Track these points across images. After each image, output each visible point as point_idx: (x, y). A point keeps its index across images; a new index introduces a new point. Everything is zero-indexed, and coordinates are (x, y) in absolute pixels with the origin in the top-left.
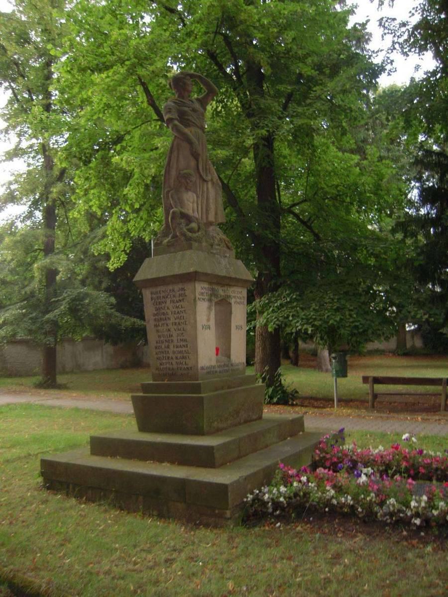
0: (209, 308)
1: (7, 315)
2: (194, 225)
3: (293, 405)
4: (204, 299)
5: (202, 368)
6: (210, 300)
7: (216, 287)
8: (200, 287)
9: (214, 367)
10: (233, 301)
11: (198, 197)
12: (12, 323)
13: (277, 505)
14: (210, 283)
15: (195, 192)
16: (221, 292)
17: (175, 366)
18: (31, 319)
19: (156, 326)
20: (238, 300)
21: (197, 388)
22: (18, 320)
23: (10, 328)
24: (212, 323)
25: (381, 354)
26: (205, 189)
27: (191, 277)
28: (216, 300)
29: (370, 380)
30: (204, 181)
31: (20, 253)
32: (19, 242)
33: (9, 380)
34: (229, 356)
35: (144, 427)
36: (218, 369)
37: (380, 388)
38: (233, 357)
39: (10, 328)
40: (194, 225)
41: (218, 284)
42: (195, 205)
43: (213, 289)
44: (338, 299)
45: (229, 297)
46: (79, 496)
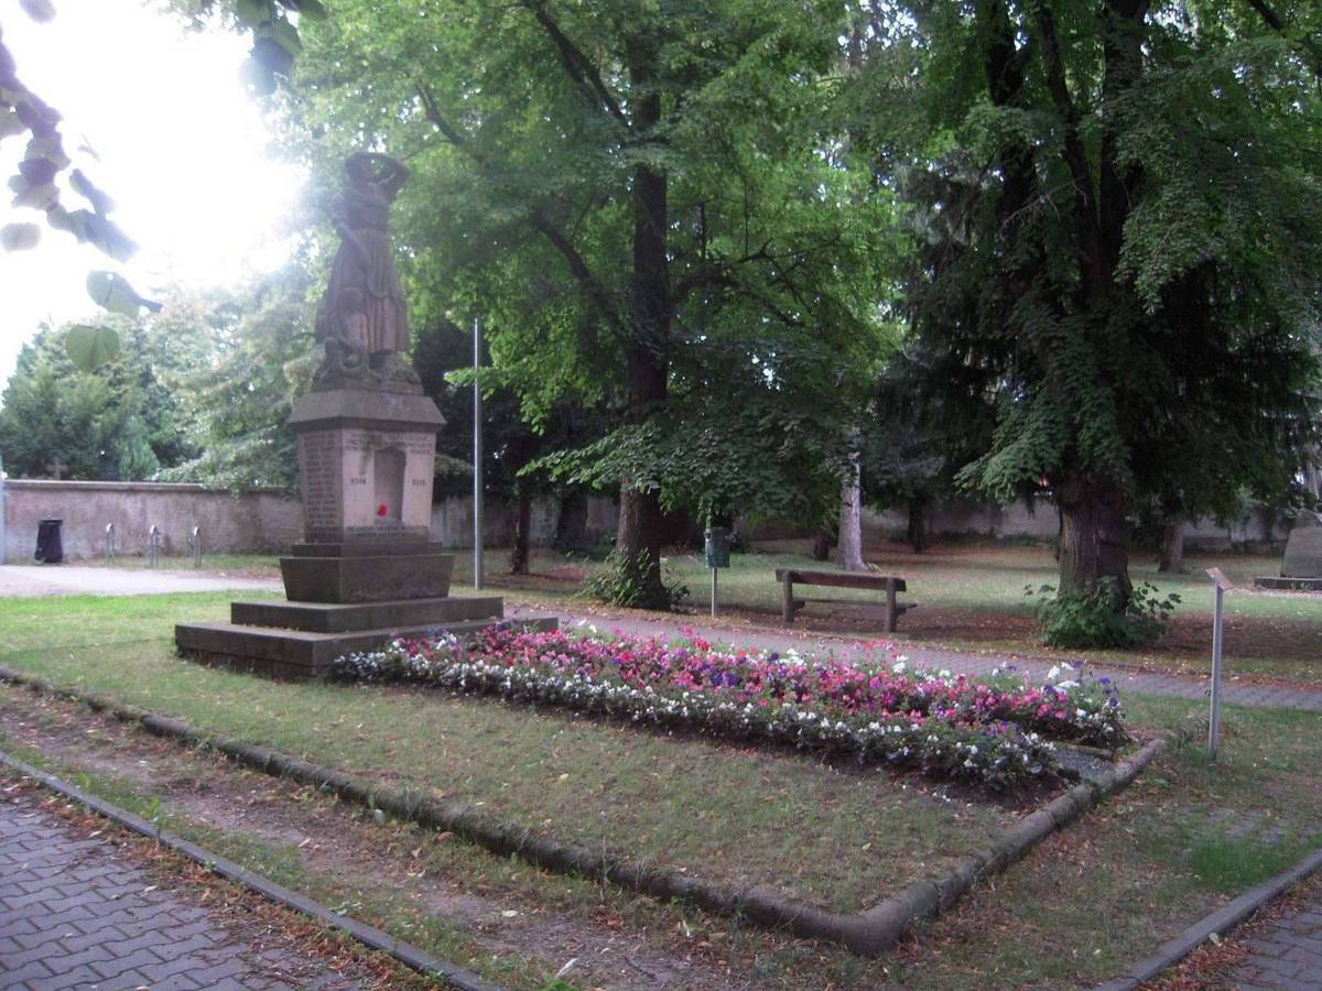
0: (365, 459)
1: (243, 448)
2: (353, 358)
3: (678, 612)
4: (355, 448)
5: (351, 529)
6: (366, 449)
7: (377, 433)
8: (347, 435)
9: (371, 528)
10: (408, 450)
11: (368, 319)
12: (249, 462)
13: (368, 668)
14: (368, 428)
15: (367, 315)
16: (387, 439)
17: (324, 526)
18: (283, 454)
19: (309, 477)
21: (336, 551)
22: (258, 455)
23: (245, 470)
24: (370, 477)
25: (1028, 545)
27: (337, 423)
28: (377, 448)
29: (785, 575)
30: (376, 299)
31: (270, 341)
32: (263, 324)
33: (264, 559)
34: (400, 517)
35: (290, 597)
36: (378, 532)
37: (800, 590)
38: (404, 519)
39: (245, 470)
40: (353, 358)
41: (378, 429)
42: (365, 330)
43: (373, 437)
44: (721, 442)
45: (402, 444)
46: (203, 662)
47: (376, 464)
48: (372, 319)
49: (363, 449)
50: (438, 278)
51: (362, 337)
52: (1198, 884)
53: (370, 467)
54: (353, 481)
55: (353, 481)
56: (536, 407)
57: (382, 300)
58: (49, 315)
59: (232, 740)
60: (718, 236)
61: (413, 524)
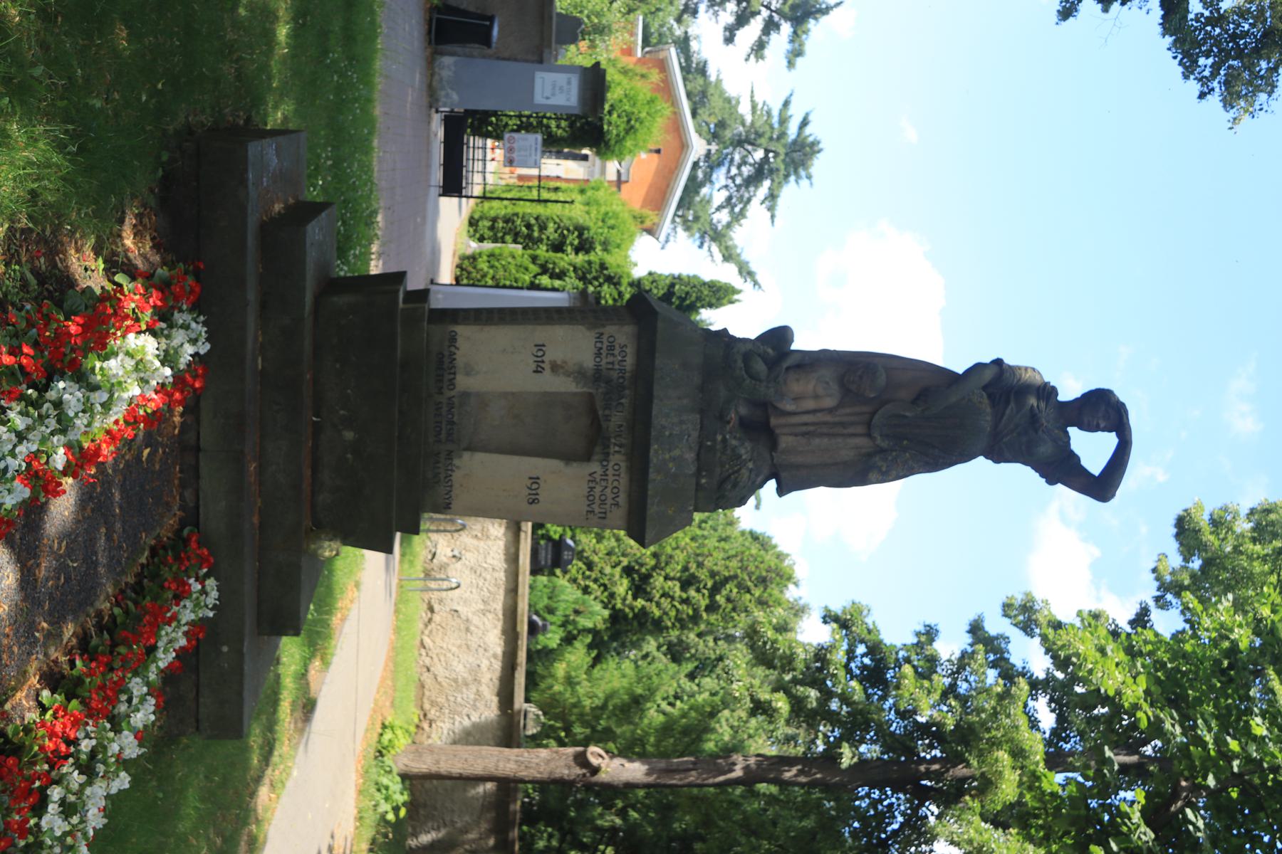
0: (580, 374)
4: (598, 354)
5: (453, 339)
6: (598, 376)
9: (452, 383)
10: (595, 467)
11: (830, 411)
16: (617, 419)
38: (466, 455)
42: (810, 404)
45: (606, 456)
47: (575, 394)
48: (828, 418)
49: (598, 370)
50: (403, 812)
51: (796, 399)
52: (602, 602)
53: (564, 385)
54: (540, 346)
55: (540, 346)
56: (570, 750)
57: (869, 435)
58: (746, 60)
59: (524, 773)
60: (62, 378)
61: (457, 476)
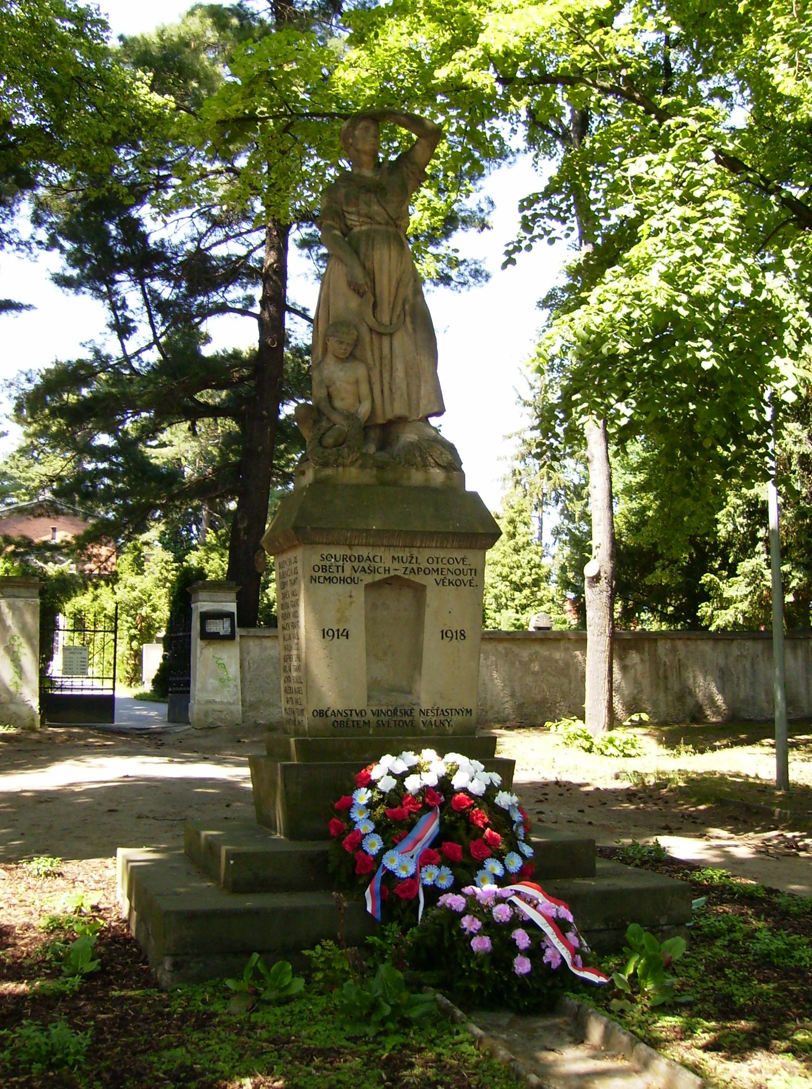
9: (361, 713)
20: (451, 577)
26: (386, 350)
